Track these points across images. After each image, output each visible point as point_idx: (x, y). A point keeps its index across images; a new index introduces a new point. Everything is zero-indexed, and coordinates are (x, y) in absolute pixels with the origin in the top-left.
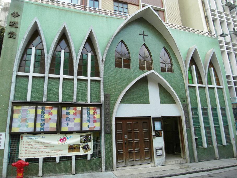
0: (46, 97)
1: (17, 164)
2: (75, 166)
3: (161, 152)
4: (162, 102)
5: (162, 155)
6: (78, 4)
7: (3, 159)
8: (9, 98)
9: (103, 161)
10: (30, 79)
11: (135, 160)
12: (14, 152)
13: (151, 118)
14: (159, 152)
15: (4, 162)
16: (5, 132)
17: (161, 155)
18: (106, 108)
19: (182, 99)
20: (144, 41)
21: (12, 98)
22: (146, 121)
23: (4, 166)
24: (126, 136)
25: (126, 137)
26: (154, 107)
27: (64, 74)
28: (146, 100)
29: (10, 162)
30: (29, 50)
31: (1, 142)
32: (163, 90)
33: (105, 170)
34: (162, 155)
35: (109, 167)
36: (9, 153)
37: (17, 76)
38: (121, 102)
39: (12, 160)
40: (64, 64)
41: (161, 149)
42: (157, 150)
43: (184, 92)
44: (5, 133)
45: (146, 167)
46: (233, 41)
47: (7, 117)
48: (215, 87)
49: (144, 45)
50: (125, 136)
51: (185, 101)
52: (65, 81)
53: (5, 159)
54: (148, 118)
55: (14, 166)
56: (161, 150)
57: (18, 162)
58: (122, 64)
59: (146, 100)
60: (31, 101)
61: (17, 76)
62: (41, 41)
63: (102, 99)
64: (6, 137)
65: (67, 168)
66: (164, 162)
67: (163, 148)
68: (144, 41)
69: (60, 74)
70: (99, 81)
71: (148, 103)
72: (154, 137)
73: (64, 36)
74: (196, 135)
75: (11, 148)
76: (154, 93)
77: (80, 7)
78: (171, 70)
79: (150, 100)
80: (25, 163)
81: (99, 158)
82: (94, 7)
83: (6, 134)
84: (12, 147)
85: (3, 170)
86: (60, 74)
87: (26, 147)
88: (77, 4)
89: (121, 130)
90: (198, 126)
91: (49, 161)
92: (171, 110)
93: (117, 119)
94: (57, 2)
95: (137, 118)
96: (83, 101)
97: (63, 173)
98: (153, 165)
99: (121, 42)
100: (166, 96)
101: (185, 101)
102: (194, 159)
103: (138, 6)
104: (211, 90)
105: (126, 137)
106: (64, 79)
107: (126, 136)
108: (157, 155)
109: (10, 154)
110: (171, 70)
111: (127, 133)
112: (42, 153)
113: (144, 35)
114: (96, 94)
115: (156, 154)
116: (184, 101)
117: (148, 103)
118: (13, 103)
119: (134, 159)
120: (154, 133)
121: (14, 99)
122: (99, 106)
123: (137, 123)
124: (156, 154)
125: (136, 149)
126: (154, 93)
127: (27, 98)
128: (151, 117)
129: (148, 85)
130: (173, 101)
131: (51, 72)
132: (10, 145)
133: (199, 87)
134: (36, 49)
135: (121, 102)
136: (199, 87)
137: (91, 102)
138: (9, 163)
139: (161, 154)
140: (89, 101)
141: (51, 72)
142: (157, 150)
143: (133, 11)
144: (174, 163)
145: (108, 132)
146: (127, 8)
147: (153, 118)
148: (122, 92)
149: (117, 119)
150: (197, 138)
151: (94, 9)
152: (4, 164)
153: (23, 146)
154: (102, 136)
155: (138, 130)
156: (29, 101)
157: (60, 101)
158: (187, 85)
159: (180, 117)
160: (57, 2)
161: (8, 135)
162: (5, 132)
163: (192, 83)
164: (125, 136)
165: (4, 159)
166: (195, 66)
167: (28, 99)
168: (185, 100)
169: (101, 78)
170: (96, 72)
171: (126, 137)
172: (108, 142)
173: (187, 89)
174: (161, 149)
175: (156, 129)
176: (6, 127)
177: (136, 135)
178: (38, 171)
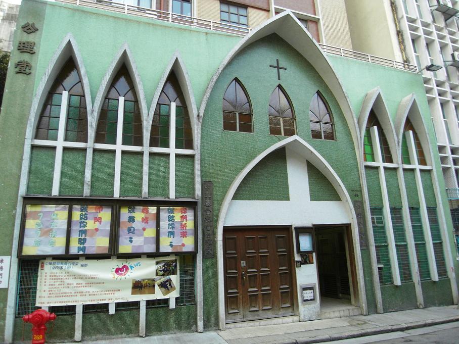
0: (88, 188)
1: (33, 317)
2: (145, 321)
3: (312, 295)
4: (314, 197)
5: (314, 300)
6: (151, 8)
7: (6, 307)
8: (18, 190)
9: (200, 312)
10: (59, 153)
11: (261, 309)
12: (27, 293)
13: (293, 228)
14: (308, 295)
15: (7, 312)
16: (11, 254)
17: (311, 300)
18: (205, 208)
19: (352, 191)
20: (279, 79)
21: (22, 190)
22: (282, 234)
23: (7, 321)
24: (244, 262)
25: (243, 264)
26: (299, 208)
27: (125, 143)
28: (283, 194)
29: (19, 314)
30: (55, 96)
31: (3, 275)
32: (316, 175)
33: (204, 328)
34: (314, 300)
35: (212, 323)
36: (18, 296)
37: (33, 147)
38: (235, 197)
39: (24, 309)
40: (124, 123)
41: (311, 288)
42: (305, 289)
43: (356, 179)
44: (10, 257)
45: (282, 323)
46: (451, 78)
47: (14, 226)
48: (415, 169)
49: (280, 86)
50: (242, 262)
51: (358, 196)
52: (126, 156)
53: (10, 307)
54: (287, 229)
55: (28, 320)
56: (312, 291)
57: (35, 313)
58: (236, 124)
59: (283, 194)
60: (60, 196)
61: (33, 147)
62: (80, 79)
63: (198, 192)
64: (12, 264)
65: (129, 326)
66: (318, 312)
67: (315, 286)
68: (279, 79)
69: (115, 144)
70: (192, 157)
71: (287, 198)
72: (298, 264)
73: (124, 70)
74: (379, 261)
75: (22, 287)
76: (297, 179)
77: (156, 13)
78: (330, 136)
79: (290, 193)
80: (48, 315)
81: (191, 304)
82: (182, 13)
83: (12, 258)
84: (24, 285)
85: (6, 328)
86: (115, 144)
87: (49, 285)
88: (150, 7)
89: (235, 252)
90: (383, 244)
91: (95, 311)
92: (331, 213)
93: (227, 230)
94: (111, 4)
95: (266, 228)
96: (161, 196)
97: (121, 334)
98: (296, 318)
99: (234, 81)
100: (322, 186)
101: (358, 196)
102: (376, 306)
103: (268, 11)
104: (409, 174)
105: (244, 265)
106: (124, 153)
107: (244, 262)
108: (305, 299)
109: (20, 297)
110: (330, 136)
111: (246, 256)
112: (81, 295)
113: (278, 68)
114: (185, 182)
115: (302, 297)
116: (355, 196)
117: (287, 198)
118: (25, 198)
119: (259, 308)
120: (297, 258)
121: (28, 191)
122: (192, 205)
123: (265, 238)
124: (302, 297)
125: (263, 289)
126: (297, 179)
127: (52, 190)
128: (293, 226)
129: (287, 164)
130: (335, 196)
131: (98, 139)
132: (19, 281)
133: (385, 168)
134: (70, 95)
135: (235, 197)
136: (385, 168)
137: (176, 198)
138: (17, 315)
139: (313, 298)
140: (172, 196)
141: (98, 139)
142: (305, 289)
143: (258, 21)
144: (337, 314)
145: (210, 255)
146: (245, 15)
147: (296, 228)
148: (237, 177)
149: (227, 230)
150: (382, 266)
151: (182, 17)
152: (8, 316)
153: (45, 282)
154: (198, 263)
155: (267, 251)
156: (56, 196)
157: (116, 195)
158: (362, 164)
159: (348, 227)
160: (111, 3)
161: (15, 261)
162: (11, 254)
163: (371, 160)
164: (242, 262)
165: (8, 307)
166: (378, 128)
167: (55, 192)
168: (359, 193)
169: (196, 151)
170: (185, 140)
171: (243, 264)
172: (210, 275)
173: (363, 171)
174: (311, 288)
175: (302, 249)
176: (12, 245)
177: (264, 261)
178: (74, 330)
